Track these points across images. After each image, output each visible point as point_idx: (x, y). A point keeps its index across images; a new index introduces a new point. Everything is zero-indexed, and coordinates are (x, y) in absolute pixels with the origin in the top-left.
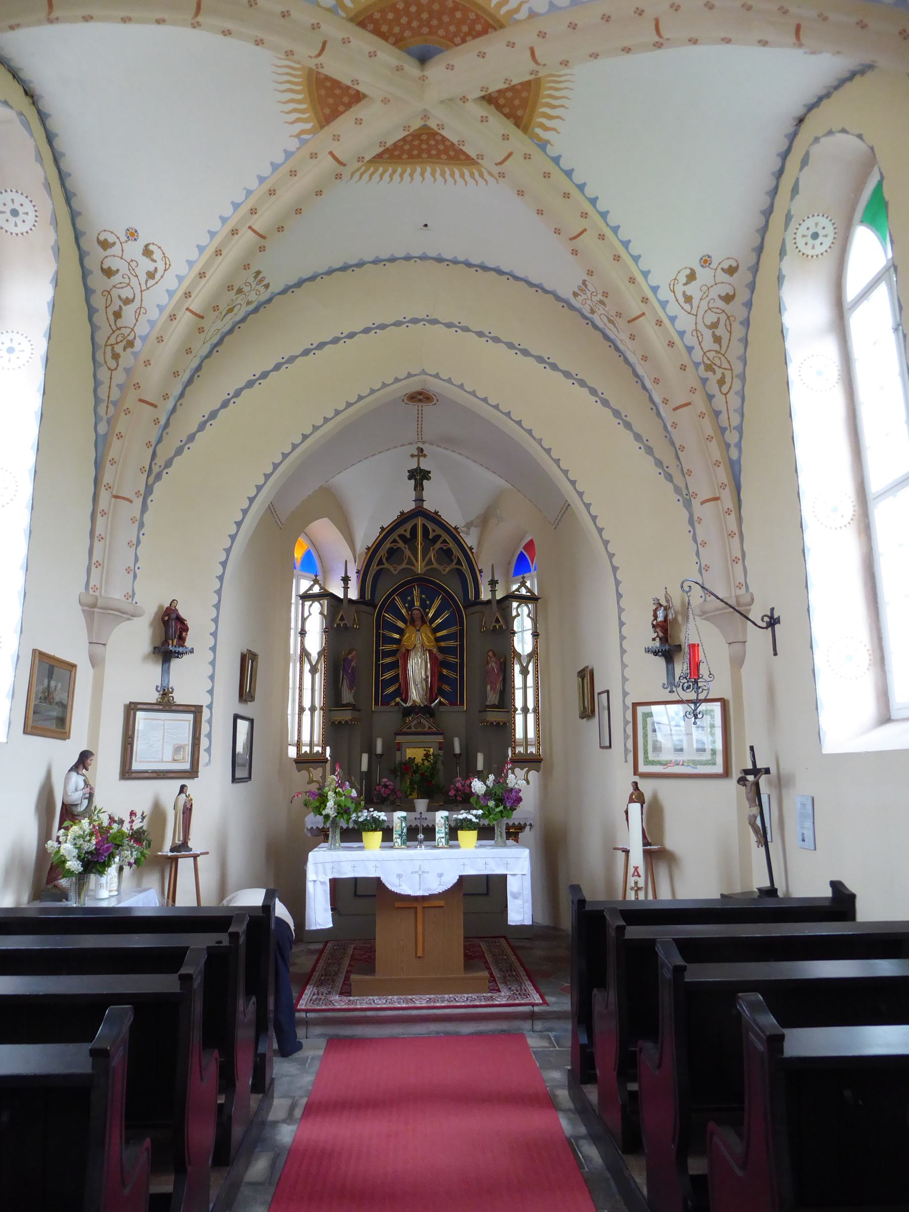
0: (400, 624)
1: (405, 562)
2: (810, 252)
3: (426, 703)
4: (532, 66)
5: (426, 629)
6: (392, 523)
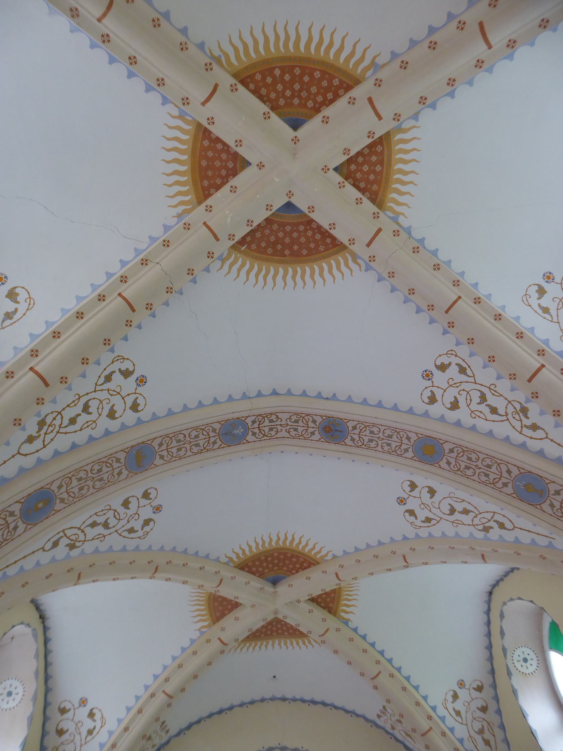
2: (527, 671)
4: (338, 582)
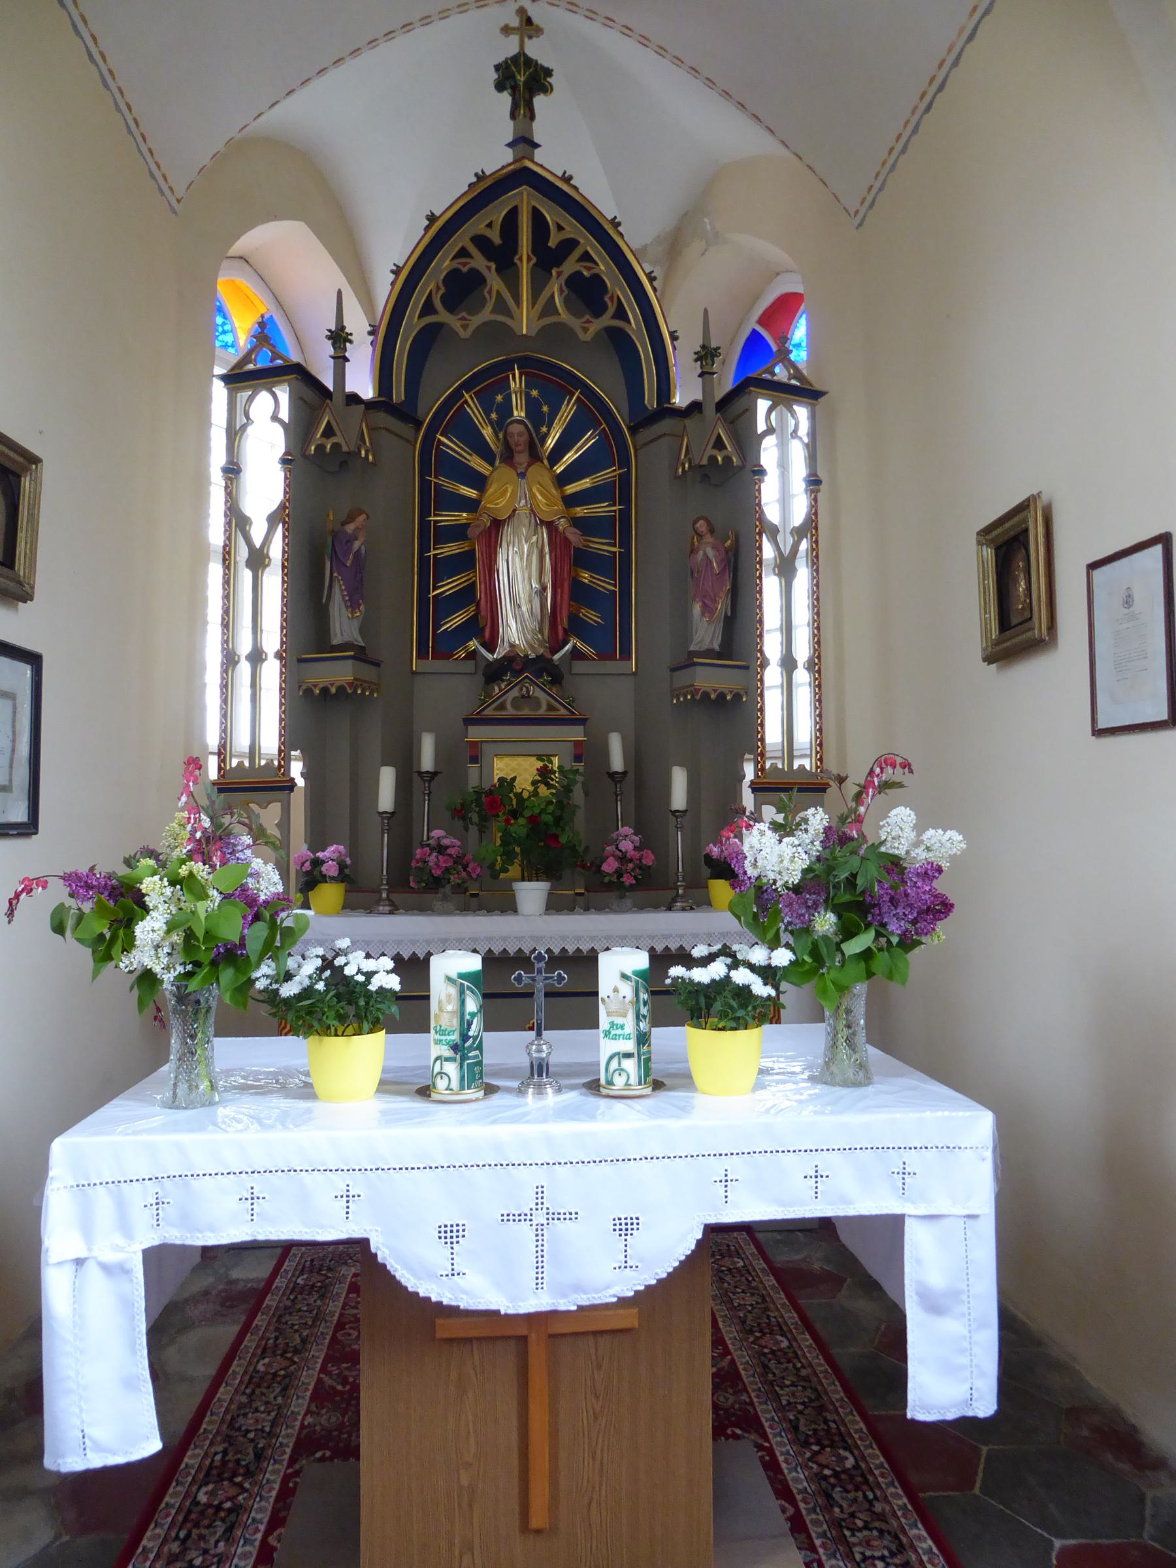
0: (477, 463)
1: (490, 305)
3: (541, 651)
5: (539, 474)
6: (460, 198)
